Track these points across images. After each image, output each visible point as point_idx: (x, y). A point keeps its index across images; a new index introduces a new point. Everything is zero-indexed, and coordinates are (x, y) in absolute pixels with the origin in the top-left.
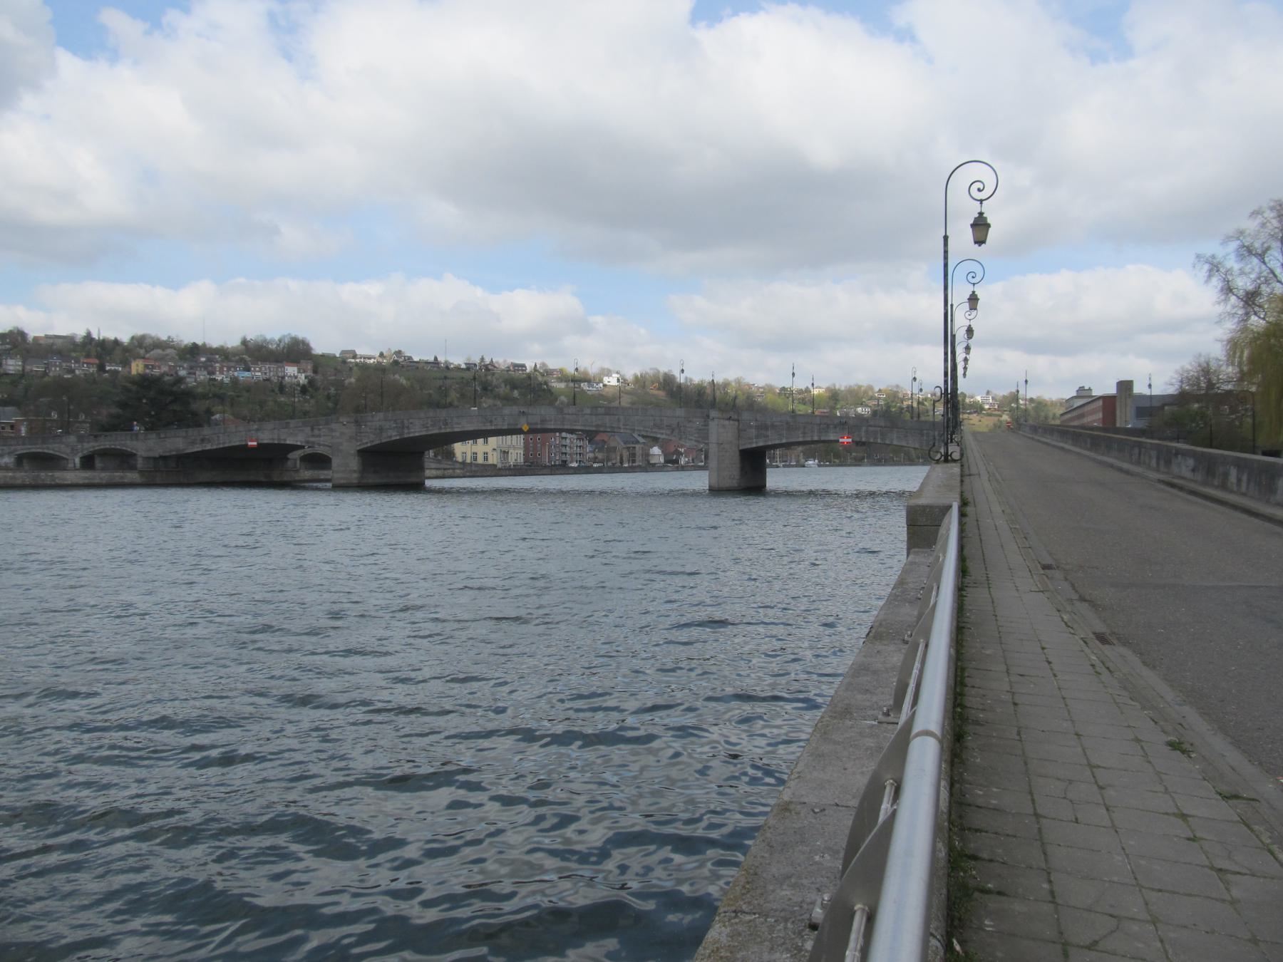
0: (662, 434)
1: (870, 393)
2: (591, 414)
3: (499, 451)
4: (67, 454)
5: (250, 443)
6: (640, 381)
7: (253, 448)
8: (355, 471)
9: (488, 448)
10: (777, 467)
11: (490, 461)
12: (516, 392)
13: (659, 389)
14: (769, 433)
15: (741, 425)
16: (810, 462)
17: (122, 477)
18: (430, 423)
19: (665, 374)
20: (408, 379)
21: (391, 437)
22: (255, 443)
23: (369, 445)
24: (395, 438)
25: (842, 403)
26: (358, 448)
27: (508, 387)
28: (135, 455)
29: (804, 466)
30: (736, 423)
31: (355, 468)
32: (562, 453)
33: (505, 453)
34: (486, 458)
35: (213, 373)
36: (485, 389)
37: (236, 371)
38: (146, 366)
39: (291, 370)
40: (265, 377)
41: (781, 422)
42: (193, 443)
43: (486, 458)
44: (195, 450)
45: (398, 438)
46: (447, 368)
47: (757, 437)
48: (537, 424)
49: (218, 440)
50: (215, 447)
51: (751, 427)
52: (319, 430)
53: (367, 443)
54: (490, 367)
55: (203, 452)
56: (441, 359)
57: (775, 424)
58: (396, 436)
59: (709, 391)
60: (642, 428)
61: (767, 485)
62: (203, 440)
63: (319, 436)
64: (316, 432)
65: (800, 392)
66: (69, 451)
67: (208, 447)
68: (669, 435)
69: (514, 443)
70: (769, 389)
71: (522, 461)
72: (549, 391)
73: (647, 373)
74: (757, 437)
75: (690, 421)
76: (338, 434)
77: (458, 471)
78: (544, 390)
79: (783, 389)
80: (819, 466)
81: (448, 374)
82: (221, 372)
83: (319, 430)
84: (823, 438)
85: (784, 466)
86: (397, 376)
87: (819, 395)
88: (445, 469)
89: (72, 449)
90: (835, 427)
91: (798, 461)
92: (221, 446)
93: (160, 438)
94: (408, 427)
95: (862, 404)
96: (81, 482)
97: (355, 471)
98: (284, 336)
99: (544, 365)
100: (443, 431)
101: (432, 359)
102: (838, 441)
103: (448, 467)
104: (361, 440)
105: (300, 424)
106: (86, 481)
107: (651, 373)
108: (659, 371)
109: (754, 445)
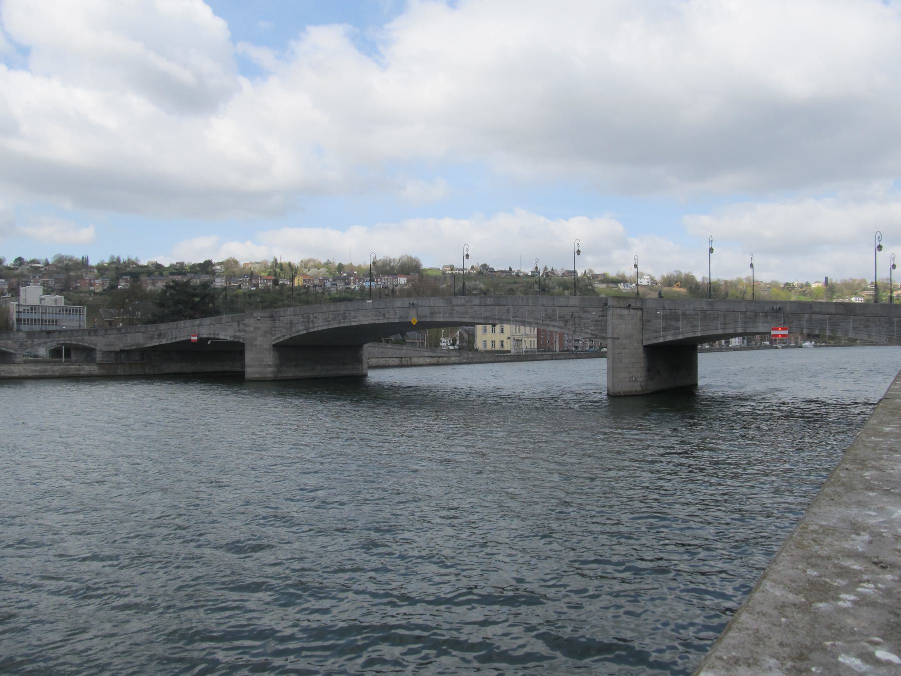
1: (863, 286)
2: (479, 306)
3: (512, 339)
4: (15, 349)
6: (669, 282)
8: (270, 366)
9: (504, 337)
10: (777, 348)
11: (505, 348)
12: (566, 291)
13: (681, 287)
14: (680, 324)
15: (645, 315)
16: (807, 343)
17: (78, 370)
18: (331, 317)
19: (686, 275)
20: (484, 283)
21: (298, 332)
22: (196, 338)
23: (282, 339)
24: (302, 333)
25: (838, 294)
26: (274, 343)
27: (561, 288)
28: (94, 349)
29: (801, 347)
30: (639, 313)
31: (271, 363)
32: (575, 340)
33: (518, 341)
34: (502, 345)
35: (349, 284)
36: (543, 290)
37: (364, 281)
38: (305, 280)
39: (403, 280)
40: (384, 286)
41: (694, 310)
42: (152, 338)
43: (493, 345)
44: (153, 344)
45: (305, 332)
46: (518, 275)
47: (665, 329)
48: (426, 317)
50: (169, 341)
51: (657, 317)
53: (280, 338)
54: (549, 274)
55: (160, 345)
56: (514, 269)
57: (687, 312)
58: (302, 330)
59: (723, 288)
60: (532, 321)
61: (700, 382)
62: (160, 336)
65: (802, 286)
66: (16, 346)
67: (164, 342)
68: (562, 328)
69: (528, 332)
70: (775, 285)
71: (536, 347)
72: (593, 291)
73: (672, 275)
74: (665, 329)
75: (585, 312)
76: (252, 329)
77: (453, 358)
78: (589, 290)
79: (787, 284)
80: (815, 346)
81: (518, 280)
82: (355, 283)
84: (748, 331)
85: (783, 347)
86: (477, 282)
87: (818, 289)
88: (439, 357)
89: (21, 345)
91: (796, 343)
92: (174, 341)
93: (121, 334)
94: (313, 322)
95: (856, 295)
96: (30, 374)
97: (270, 366)
98: (403, 257)
99: (591, 271)
100: (342, 325)
101: (507, 269)
102: (770, 333)
103: (443, 354)
104: (275, 335)
105: (229, 320)
106: (37, 374)
107: (675, 274)
108: (681, 273)
109: (661, 340)
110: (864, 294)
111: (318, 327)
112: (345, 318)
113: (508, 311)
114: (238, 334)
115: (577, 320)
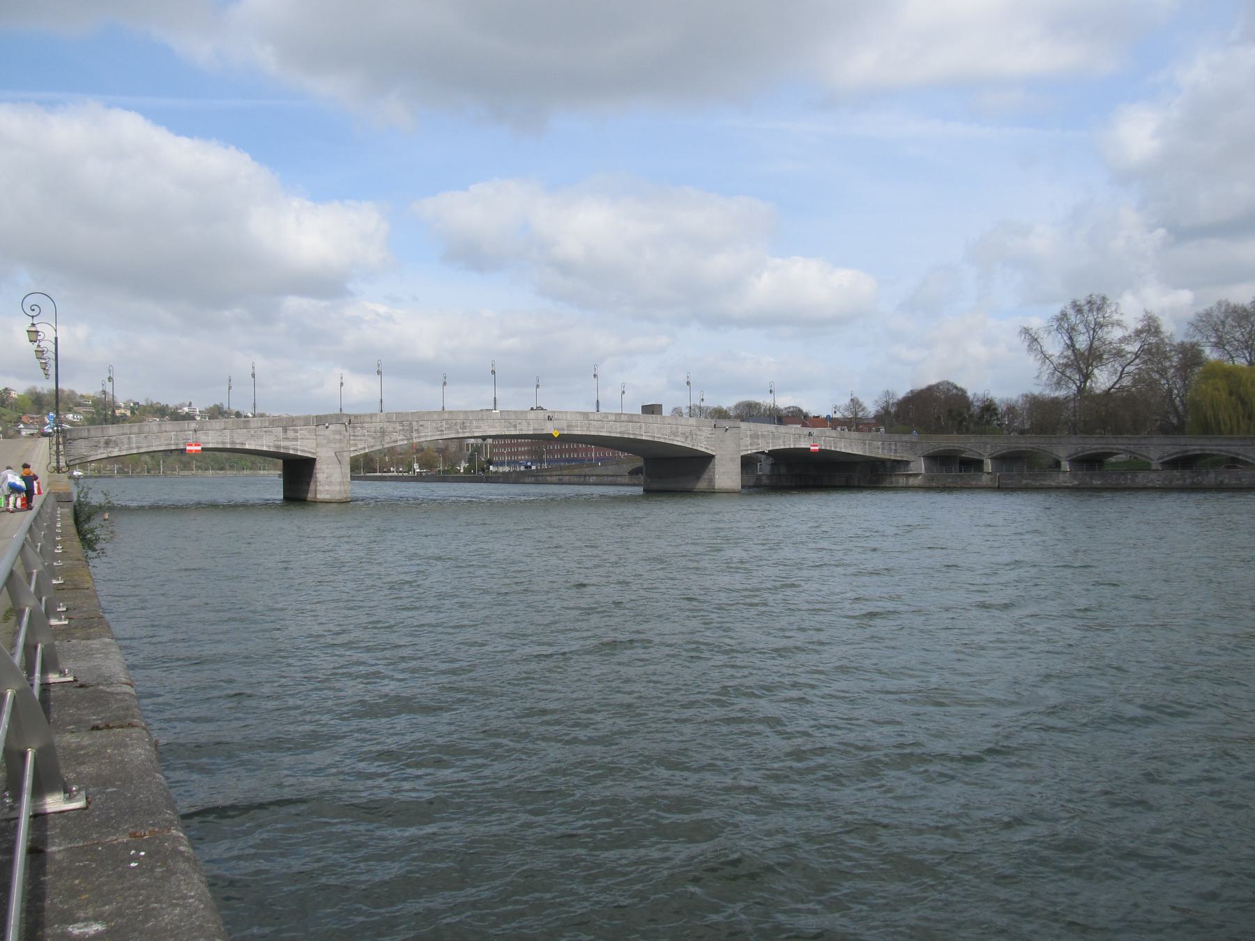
5: (812, 448)
7: (815, 453)
21: (396, 441)
22: (817, 448)
52: (296, 431)
58: (402, 440)
62: (107, 443)
63: (296, 439)
64: (291, 434)
75: (700, 430)
83: (296, 431)
104: (356, 445)
110: (81, 410)
111: (426, 436)
112: (465, 427)
113: (641, 427)
114: (282, 444)
115: (694, 436)
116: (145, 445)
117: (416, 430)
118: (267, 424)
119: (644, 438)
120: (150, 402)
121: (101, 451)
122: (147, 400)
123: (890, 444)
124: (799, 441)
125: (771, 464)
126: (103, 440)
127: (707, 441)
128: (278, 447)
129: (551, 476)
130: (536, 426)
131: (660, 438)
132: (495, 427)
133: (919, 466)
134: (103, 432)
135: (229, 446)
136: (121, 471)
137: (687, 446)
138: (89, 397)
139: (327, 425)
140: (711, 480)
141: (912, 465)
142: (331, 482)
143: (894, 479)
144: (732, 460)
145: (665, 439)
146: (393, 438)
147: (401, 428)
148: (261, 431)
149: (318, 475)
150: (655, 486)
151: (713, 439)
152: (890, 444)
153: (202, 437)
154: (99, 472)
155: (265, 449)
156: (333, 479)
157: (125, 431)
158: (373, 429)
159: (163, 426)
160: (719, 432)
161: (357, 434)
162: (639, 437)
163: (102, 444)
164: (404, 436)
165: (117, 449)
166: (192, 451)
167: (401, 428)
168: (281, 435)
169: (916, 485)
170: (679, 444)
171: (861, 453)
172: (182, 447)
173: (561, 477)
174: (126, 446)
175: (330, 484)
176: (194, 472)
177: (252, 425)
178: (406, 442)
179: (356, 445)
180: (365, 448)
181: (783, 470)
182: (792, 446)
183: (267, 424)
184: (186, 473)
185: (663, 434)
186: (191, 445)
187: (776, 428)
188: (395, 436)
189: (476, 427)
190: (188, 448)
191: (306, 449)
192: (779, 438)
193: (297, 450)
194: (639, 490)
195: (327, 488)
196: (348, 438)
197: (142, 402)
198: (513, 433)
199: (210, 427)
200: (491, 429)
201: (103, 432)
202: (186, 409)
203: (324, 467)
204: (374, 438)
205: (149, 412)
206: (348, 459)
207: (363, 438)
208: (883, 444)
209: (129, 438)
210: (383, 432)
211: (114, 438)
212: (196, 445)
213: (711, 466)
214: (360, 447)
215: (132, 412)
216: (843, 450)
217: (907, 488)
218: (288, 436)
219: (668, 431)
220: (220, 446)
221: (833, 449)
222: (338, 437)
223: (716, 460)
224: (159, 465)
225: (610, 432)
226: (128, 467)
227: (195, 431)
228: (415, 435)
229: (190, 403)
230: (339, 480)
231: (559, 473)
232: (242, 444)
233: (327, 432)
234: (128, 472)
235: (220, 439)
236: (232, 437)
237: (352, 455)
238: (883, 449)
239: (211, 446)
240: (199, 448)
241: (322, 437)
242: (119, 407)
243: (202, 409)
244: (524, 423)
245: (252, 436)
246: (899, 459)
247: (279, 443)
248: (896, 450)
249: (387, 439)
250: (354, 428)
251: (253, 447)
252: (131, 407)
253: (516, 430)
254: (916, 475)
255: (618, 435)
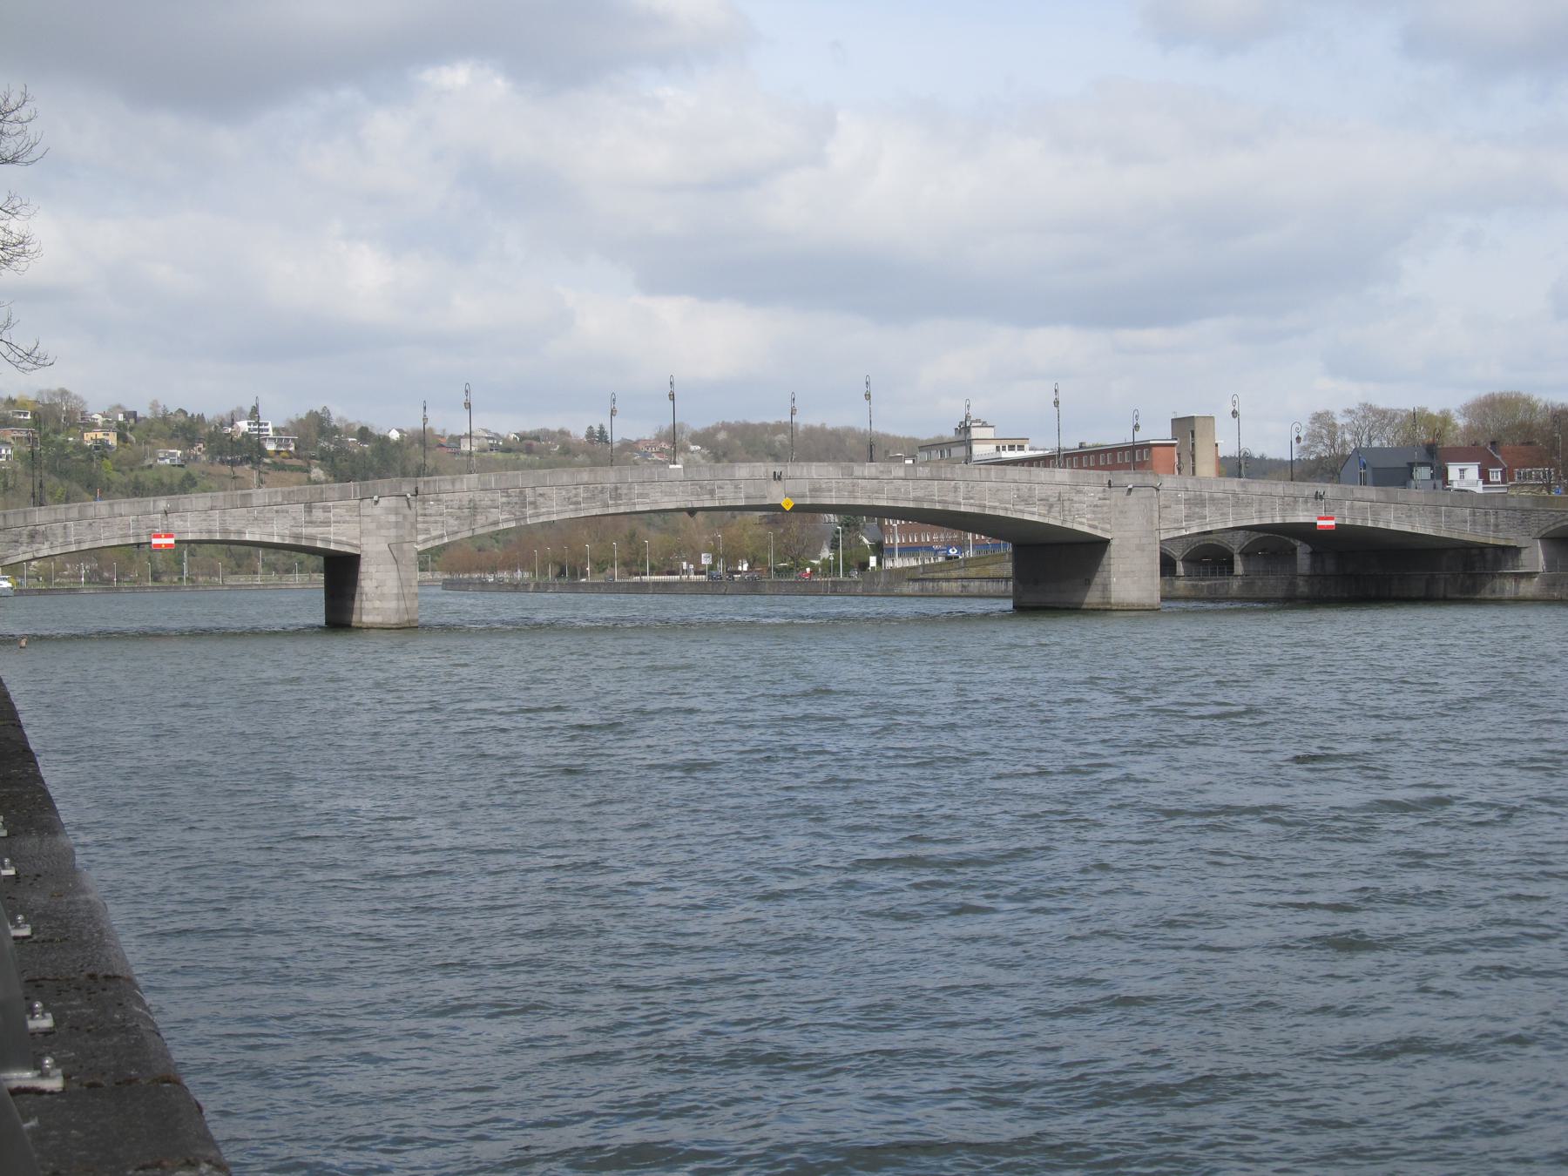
0: (1033, 513)
5: (1320, 523)
21: (496, 523)
22: (1332, 523)
49: (66, 535)
52: (326, 510)
62: (32, 536)
63: (327, 523)
64: (318, 514)
75: (1079, 492)
83: (326, 510)
90: (1306, 502)
104: (427, 531)
111: (549, 513)
113: (956, 489)
114: (304, 531)
115: (1067, 504)
116: (89, 537)
117: (531, 503)
118: (279, 499)
119: (962, 509)
120: (160, 411)
121: (23, 548)
122: (154, 405)
123: (1486, 514)
124: (1294, 509)
125: (1311, 553)
126: (26, 532)
127: (1094, 512)
128: (298, 536)
129: (948, 580)
130: (752, 491)
131: (995, 508)
132: (674, 495)
133: (1536, 558)
134: (25, 518)
135: (218, 537)
136: (94, 577)
137: (1052, 522)
138: (24, 405)
139: (376, 498)
140: (1106, 587)
141: (1524, 555)
142: (383, 594)
143: (1498, 582)
144: (1141, 548)
145: (1006, 509)
146: (492, 518)
147: (504, 500)
148: (269, 511)
149: (363, 583)
150: (1029, 599)
151: (1105, 509)
152: (1486, 514)
153: (176, 523)
154: (48, 579)
155: (276, 540)
156: (386, 590)
157: (59, 517)
158: (456, 504)
159: (116, 507)
160: (1117, 495)
161: (427, 512)
162: (952, 508)
163: (25, 539)
164: (510, 513)
165: (47, 545)
166: (160, 545)
167: (504, 500)
168: (303, 517)
169: (1529, 595)
170: (1035, 518)
171: (1430, 531)
172: (144, 539)
173: (965, 583)
174: (60, 540)
175: (382, 597)
176: (258, 580)
177: (255, 501)
178: (513, 525)
179: (427, 531)
180: (442, 536)
181: (1330, 566)
182: (1278, 520)
183: (279, 499)
184: (242, 579)
185: (1001, 501)
186: (159, 536)
187: (1243, 485)
188: (495, 514)
189: (640, 495)
190: (155, 541)
191: (344, 539)
192: (1249, 504)
193: (328, 541)
194: (1008, 605)
195: (377, 604)
196: (412, 519)
197: (144, 412)
198: (708, 504)
199: (189, 507)
200: (666, 499)
201: (25, 518)
202: (243, 426)
203: (372, 569)
204: (458, 518)
205: (160, 435)
206: (414, 555)
207: (438, 518)
208: (1474, 514)
209: (65, 527)
210: (474, 508)
211: (43, 527)
212: (167, 536)
213: (1105, 561)
214: (434, 533)
215: (122, 437)
216: (1393, 527)
217: (1519, 601)
218: (314, 519)
219: (1014, 495)
220: (205, 537)
221: (1370, 524)
222: (392, 518)
223: (1113, 550)
224: (180, 563)
225: (894, 499)
226: (110, 569)
227: (166, 513)
228: (529, 511)
229: (255, 410)
230: (395, 591)
231: (962, 573)
232: (240, 532)
233: (377, 510)
234: (110, 581)
235: (204, 526)
236: (223, 522)
237: (420, 548)
238: (1474, 523)
239: (190, 537)
240: (171, 541)
241: (368, 519)
242: (92, 426)
243: (281, 425)
244: (729, 487)
245: (256, 519)
246: (1503, 543)
247: (299, 530)
248: (1497, 526)
249: (481, 519)
250: (424, 501)
251: (257, 538)
252: (119, 425)
253: (713, 498)
254: (1530, 575)
255: (911, 505)
